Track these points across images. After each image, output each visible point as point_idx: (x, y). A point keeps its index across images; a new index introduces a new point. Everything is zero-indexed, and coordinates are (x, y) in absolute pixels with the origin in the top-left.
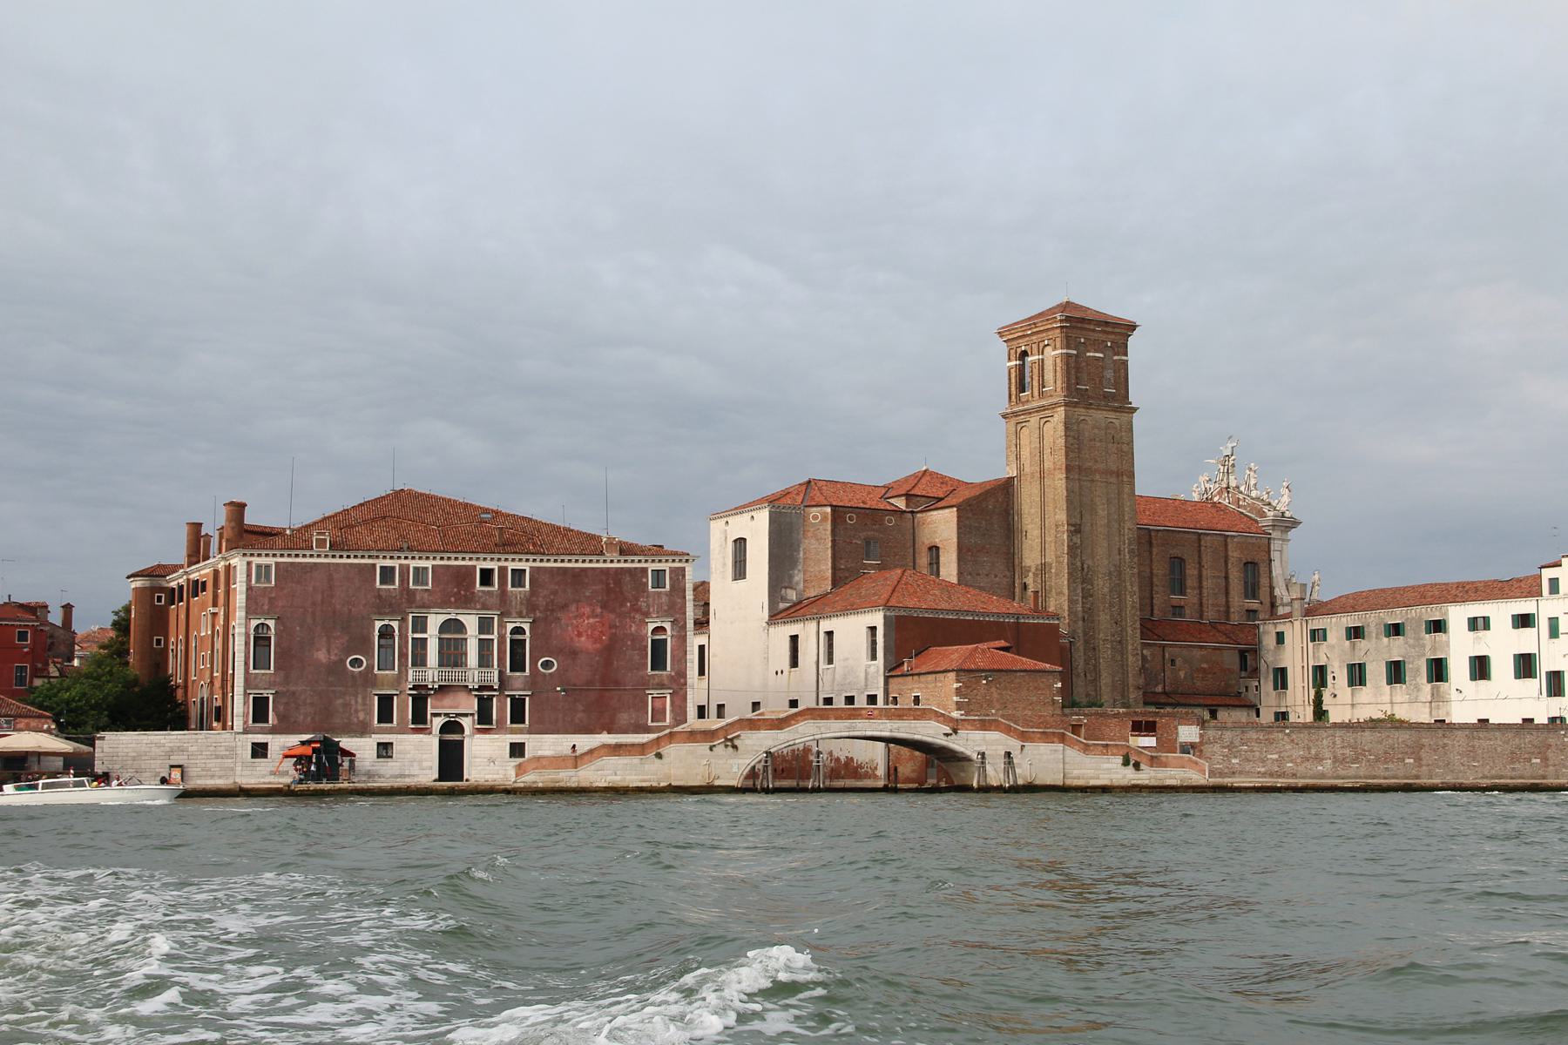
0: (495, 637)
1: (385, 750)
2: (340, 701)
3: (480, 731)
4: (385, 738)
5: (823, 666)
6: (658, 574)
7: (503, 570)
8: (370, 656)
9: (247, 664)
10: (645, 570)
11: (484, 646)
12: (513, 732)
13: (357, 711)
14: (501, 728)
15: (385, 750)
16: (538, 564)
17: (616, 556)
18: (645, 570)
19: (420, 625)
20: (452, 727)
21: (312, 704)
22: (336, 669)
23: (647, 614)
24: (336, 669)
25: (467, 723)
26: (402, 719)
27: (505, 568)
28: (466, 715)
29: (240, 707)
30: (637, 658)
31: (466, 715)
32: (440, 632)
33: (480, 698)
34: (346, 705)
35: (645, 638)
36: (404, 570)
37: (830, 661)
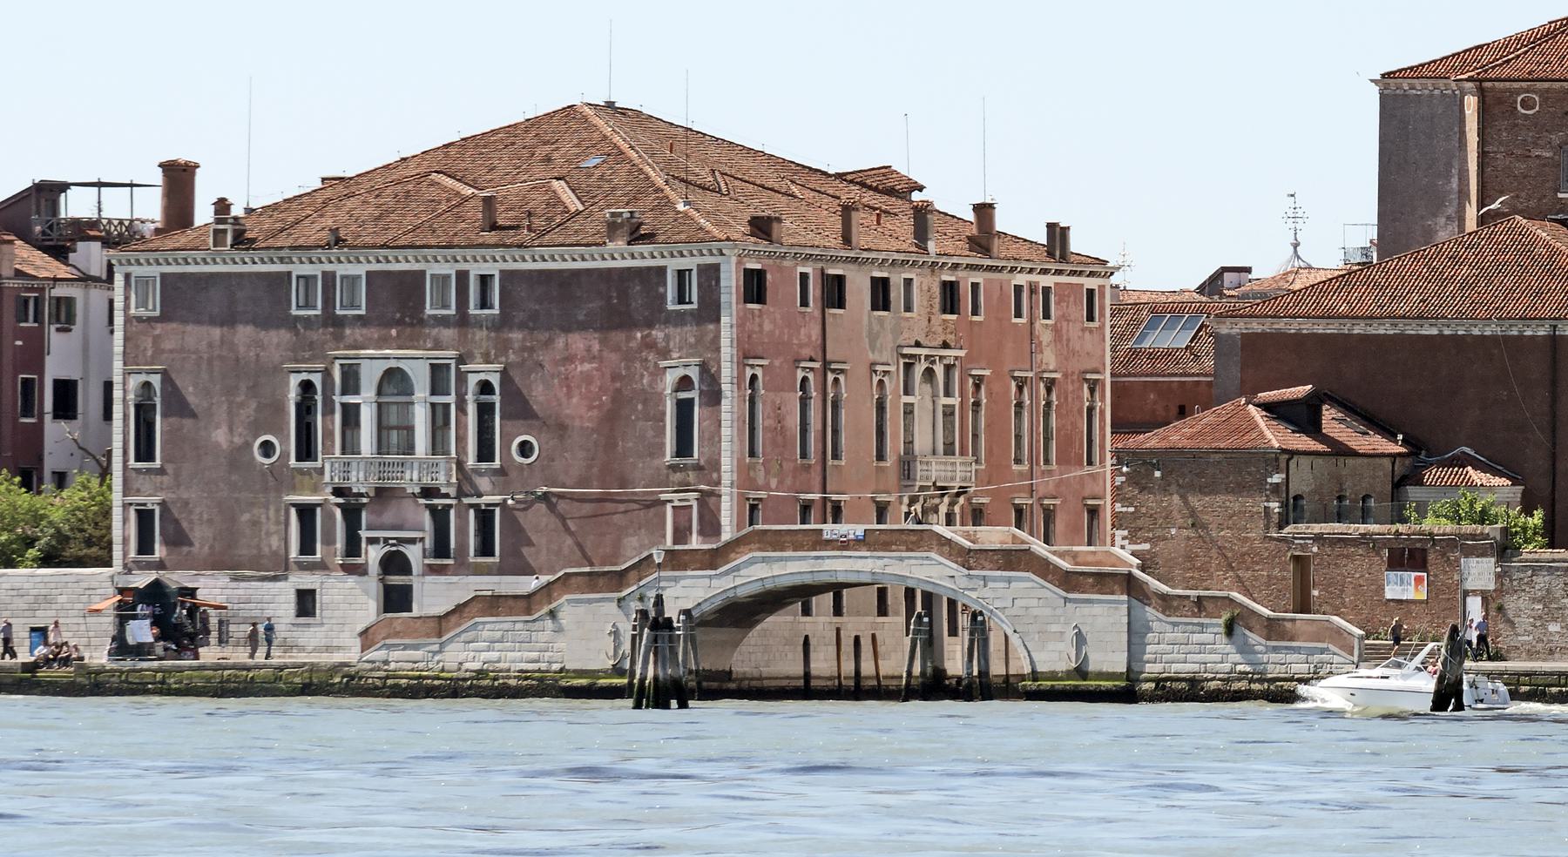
0: (451, 399)
1: (306, 603)
2: (246, 517)
3: (433, 570)
4: (307, 581)
5: (830, 462)
6: (308, 280)
7: (462, 276)
8: (284, 440)
9: (125, 452)
10: (662, 271)
11: (439, 417)
12: (479, 571)
13: (268, 534)
14: (463, 568)
15: (306, 603)
16: (375, 267)
17: (619, 245)
18: (662, 271)
19: (351, 382)
20: (394, 563)
21: (210, 521)
22: (237, 458)
23: (665, 354)
24: (237, 458)
25: (414, 553)
26: (462, 518)
27: (333, 274)
28: (412, 541)
29: (122, 529)
30: (650, 433)
31: (412, 541)
32: (379, 393)
33: (433, 510)
34: (255, 523)
35: (660, 398)
36: (329, 278)
37: (836, 456)
